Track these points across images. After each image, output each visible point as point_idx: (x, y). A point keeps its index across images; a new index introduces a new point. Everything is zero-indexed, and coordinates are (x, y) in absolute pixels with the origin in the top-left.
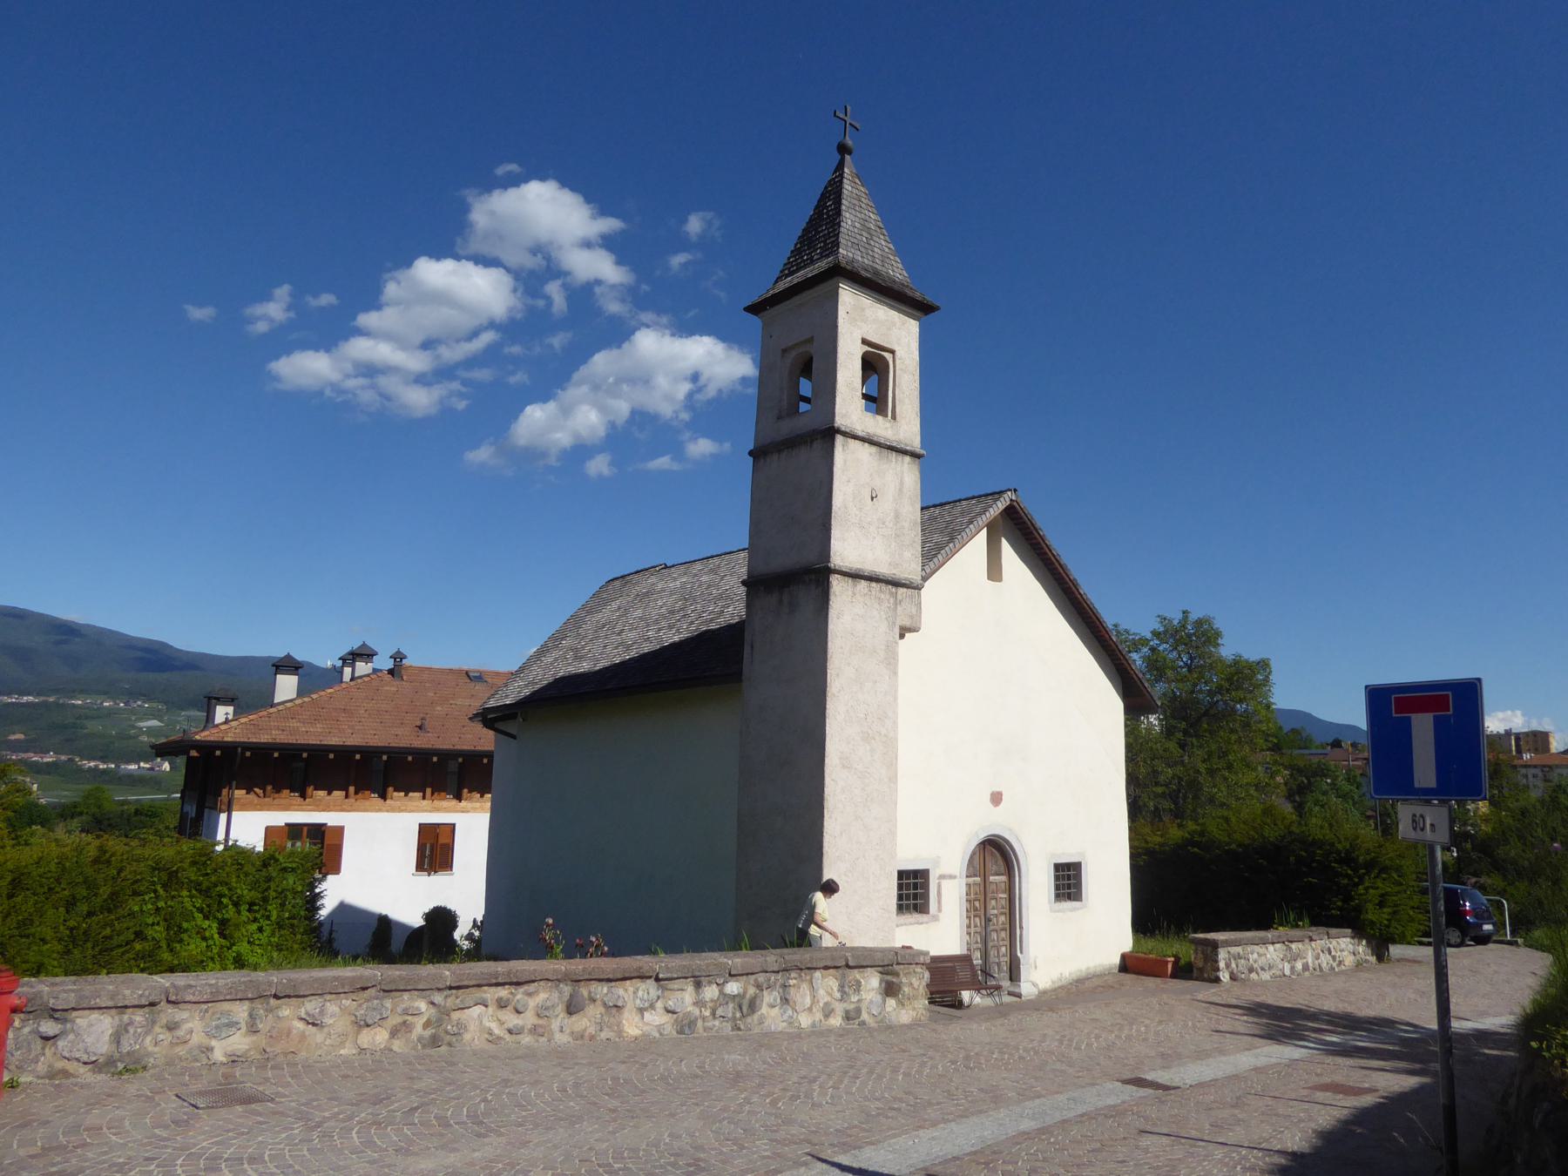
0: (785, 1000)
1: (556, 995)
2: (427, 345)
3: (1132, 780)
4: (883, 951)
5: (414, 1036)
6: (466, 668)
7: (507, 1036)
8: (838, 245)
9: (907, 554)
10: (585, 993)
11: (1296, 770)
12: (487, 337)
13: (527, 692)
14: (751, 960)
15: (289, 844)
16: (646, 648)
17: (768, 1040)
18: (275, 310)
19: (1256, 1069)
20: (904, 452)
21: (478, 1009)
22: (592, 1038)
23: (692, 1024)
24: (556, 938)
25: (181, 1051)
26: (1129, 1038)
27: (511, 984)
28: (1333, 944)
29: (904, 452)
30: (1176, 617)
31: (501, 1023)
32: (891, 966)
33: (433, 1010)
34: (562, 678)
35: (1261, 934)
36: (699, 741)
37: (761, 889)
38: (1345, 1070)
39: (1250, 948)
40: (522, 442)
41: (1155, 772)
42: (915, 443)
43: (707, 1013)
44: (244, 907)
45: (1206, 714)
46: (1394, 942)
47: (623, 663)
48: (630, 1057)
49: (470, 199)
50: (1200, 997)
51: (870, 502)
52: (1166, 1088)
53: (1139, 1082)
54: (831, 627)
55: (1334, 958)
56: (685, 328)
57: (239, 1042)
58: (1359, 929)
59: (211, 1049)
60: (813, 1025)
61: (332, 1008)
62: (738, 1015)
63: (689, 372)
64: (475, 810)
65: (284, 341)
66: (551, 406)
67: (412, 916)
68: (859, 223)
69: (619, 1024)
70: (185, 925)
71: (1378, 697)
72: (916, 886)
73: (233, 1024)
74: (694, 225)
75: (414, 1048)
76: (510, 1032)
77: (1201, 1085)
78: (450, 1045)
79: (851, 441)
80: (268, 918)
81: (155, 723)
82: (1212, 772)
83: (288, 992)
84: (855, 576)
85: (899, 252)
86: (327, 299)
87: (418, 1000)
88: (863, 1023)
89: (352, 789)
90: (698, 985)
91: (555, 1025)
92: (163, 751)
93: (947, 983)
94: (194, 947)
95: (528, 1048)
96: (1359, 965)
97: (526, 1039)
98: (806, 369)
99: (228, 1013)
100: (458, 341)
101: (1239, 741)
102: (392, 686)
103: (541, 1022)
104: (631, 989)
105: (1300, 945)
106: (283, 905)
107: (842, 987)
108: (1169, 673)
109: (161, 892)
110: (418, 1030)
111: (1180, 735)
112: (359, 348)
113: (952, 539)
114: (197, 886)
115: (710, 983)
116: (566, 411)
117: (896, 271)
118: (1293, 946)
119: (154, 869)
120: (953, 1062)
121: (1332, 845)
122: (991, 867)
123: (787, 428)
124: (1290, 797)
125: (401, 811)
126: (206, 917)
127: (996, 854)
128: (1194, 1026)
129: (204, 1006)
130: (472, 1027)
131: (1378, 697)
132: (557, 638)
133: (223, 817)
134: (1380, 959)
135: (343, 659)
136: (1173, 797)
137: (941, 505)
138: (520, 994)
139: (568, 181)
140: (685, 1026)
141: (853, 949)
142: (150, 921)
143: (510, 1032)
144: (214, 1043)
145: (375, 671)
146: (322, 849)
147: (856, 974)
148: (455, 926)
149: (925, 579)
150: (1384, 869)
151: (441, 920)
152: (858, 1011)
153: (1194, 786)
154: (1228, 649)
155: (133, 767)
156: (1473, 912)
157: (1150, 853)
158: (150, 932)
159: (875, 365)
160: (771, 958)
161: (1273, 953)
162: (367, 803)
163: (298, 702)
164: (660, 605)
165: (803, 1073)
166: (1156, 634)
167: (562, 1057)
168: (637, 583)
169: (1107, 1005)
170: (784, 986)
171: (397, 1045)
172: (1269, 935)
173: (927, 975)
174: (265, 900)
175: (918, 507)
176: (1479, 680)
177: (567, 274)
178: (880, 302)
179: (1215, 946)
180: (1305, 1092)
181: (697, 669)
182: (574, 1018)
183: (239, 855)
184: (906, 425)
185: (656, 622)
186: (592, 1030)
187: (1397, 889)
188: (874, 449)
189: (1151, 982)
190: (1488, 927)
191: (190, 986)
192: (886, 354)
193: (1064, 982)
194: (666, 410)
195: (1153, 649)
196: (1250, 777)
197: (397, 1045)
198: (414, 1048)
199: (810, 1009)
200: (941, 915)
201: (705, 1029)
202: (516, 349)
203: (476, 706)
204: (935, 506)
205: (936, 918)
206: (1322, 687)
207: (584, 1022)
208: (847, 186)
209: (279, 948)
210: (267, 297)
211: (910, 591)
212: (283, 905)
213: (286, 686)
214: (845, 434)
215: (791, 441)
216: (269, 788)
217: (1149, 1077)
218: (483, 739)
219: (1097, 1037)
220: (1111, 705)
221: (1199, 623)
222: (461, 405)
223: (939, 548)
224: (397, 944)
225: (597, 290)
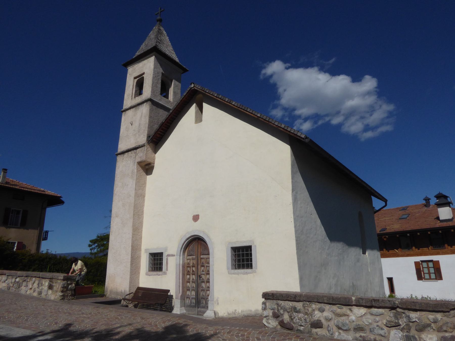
79: (127, 112)
127: (196, 245)
188: (134, 109)
193: (237, 315)
205: (165, 273)
214: (329, 80)
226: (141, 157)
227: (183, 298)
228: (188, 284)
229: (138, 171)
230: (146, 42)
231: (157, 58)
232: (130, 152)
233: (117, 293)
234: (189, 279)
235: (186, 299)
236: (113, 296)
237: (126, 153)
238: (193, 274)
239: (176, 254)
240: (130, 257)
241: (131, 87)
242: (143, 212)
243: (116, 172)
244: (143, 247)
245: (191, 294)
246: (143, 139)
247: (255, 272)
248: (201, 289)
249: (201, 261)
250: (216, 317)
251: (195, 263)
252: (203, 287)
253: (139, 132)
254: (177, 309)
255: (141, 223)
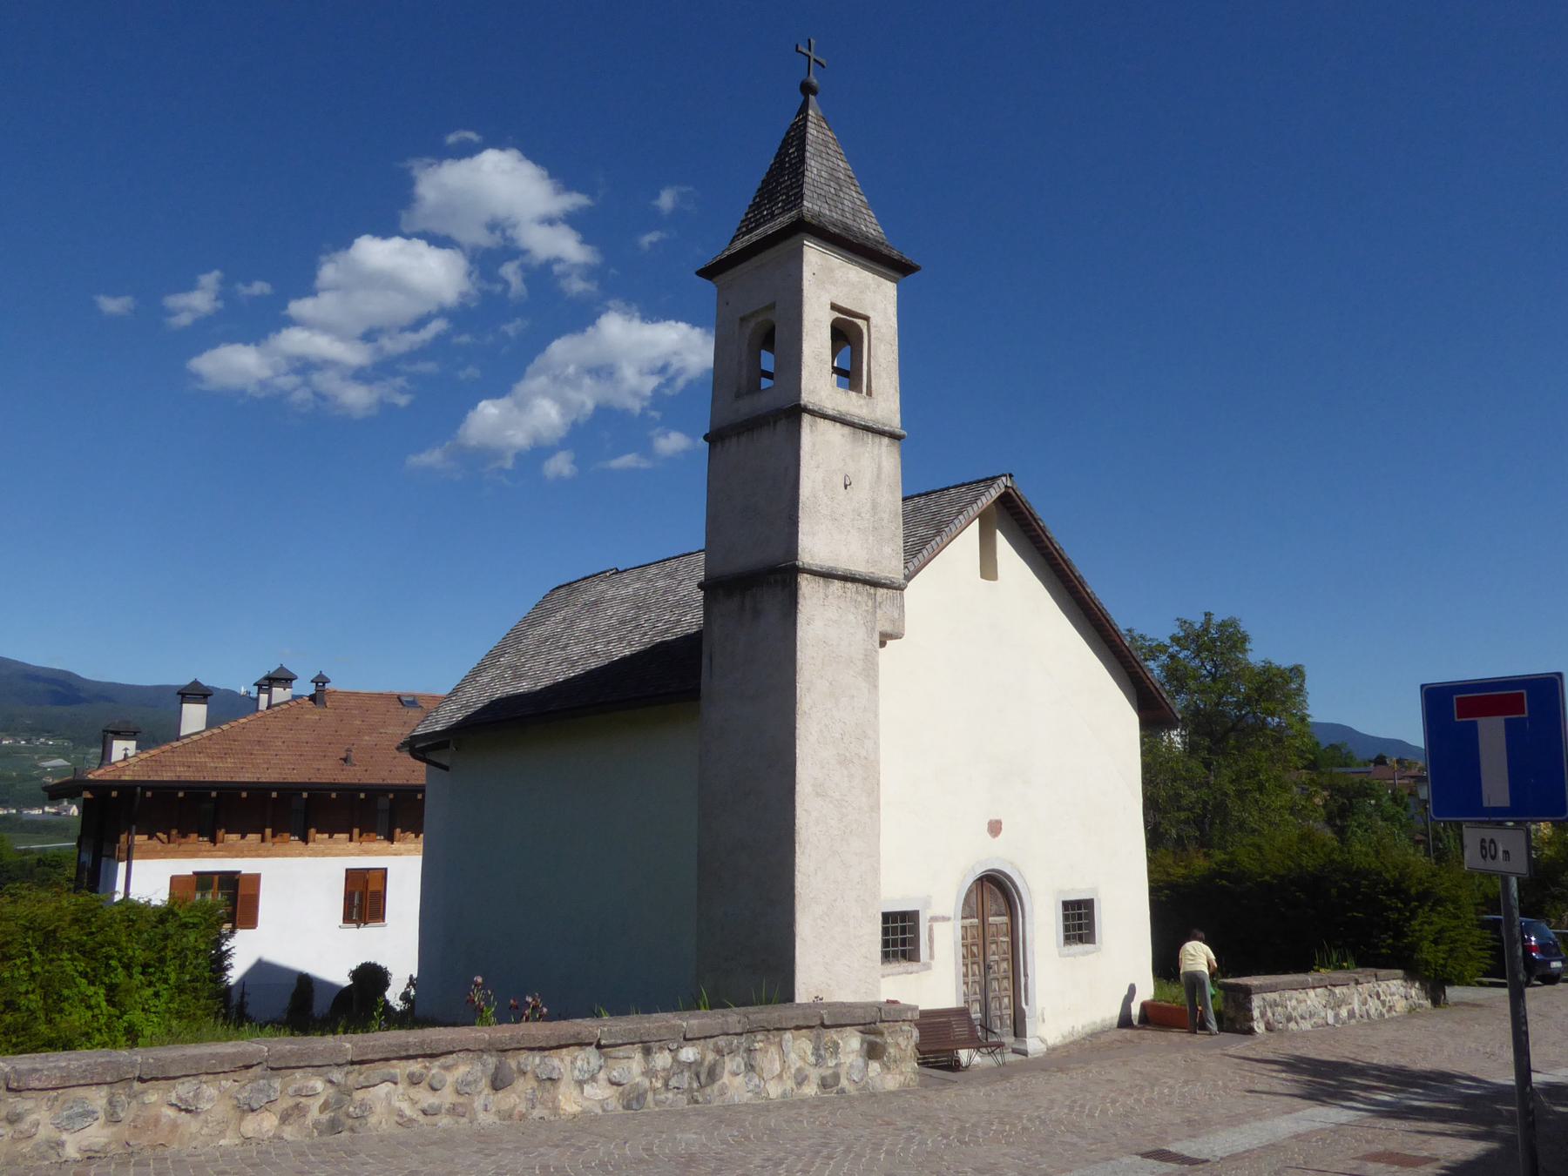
0: (750, 1067)
1: (479, 1067)
2: (369, 336)
3: (1151, 805)
4: (865, 1006)
5: (309, 1121)
6: (397, 691)
7: (421, 1118)
8: (801, 196)
9: (887, 550)
10: (513, 1065)
11: (1336, 790)
12: (437, 326)
13: (459, 716)
14: (706, 1021)
15: (198, 896)
16: (593, 664)
17: (730, 1114)
18: (200, 300)
19: (1297, 1136)
20: (882, 433)
21: (385, 1088)
22: (523, 1117)
23: (640, 1097)
24: (487, 999)
25: (25, 1147)
26: (1150, 1101)
27: (424, 1056)
28: (1382, 987)
29: (882, 433)
30: (1198, 621)
31: (414, 1102)
32: (873, 1024)
33: (331, 1090)
34: (500, 700)
35: (1301, 977)
36: (649, 772)
37: (721, 938)
38: (1399, 1135)
39: (1287, 994)
40: (473, 443)
41: (1178, 795)
42: (894, 421)
43: (659, 1084)
44: (137, 970)
45: (1233, 729)
46: (1451, 983)
47: (567, 681)
48: (566, 1139)
49: (415, 172)
50: (1231, 1051)
51: (844, 493)
52: (1192, 1161)
53: (1162, 1155)
54: (800, 633)
55: (1383, 1003)
56: (653, 313)
57: (97, 1134)
58: (1412, 971)
59: (61, 1144)
60: (784, 1095)
61: (209, 1090)
62: (695, 1085)
63: (660, 364)
64: (409, 852)
65: (208, 333)
66: (506, 402)
67: (339, 974)
68: (824, 164)
69: (555, 1099)
70: (66, 992)
71: (1437, 699)
72: (904, 930)
73: (89, 1114)
74: (666, 200)
75: (310, 1135)
76: (425, 1112)
77: (1234, 1157)
78: (352, 1130)
79: (820, 421)
80: (166, 981)
81: (60, 762)
82: (1241, 794)
83: (155, 1074)
84: (827, 575)
85: (873, 204)
86: (260, 288)
87: (316, 1077)
88: (843, 1091)
89: (268, 831)
90: (647, 1052)
91: (478, 1103)
92: (56, 794)
93: (940, 1042)
94: (77, 1017)
95: (445, 1130)
96: (1412, 1010)
97: (444, 1121)
98: (768, 339)
99: (83, 1100)
100: (403, 330)
101: (1271, 759)
102: (313, 714)
103: (461, 1100)
104: (568, 1059)
105: (1345, 989)
106: (182, 966)
107: (816, 1049)
108: (1191, 683)
109: (36, 955)
110: (314, 1114)
111: (1204, 754)
112: (295, 341)
113: (939, 532)
114: (80, 947)
115: (661, 1049)
116: (523, 405)
117: (870, 227)
118: (1337, 990)
119: (28, 929)
120: (945, 1136)
121: (1379, 874)
122: (991, 906)
123: (747, 407)
124: (1330, 821)
125: (324, 855)
126: (91, 983)
127: (995, 893)
128: (1225, 1087)
129: (54, 1093)
130: (379, 1108)
131: (1437, 699)
132: (494, 655)
133: (122, 866)
134: (1436, 1002)
135: (259, 685)
136: (1199, 822)
137: (927, 494)
138: (435, 1068)
139: (531, 153)
140: (633, 1099)
141: (830, 1005)
142: (22, 989)
143: (425, 1112)
144: (65, 1136)
145: (294, 698)
146: (236, 901)
147: (833, 1034)
148: (386, 985)
149: (908, 578)
150: (1439, 901)
151: (371, 978)
152: (836, 1077)
153: (1221, 809)
154: (1257, 655)
155: (37, 812)
156: (1542, 948)
157: (1172, 886)
158: (23, 1001)
159: (846, 334)
160: (733, 1017)
161: (1313, 999)
162: (286, 847)
163: (207, 734)
164: (612, 613)
165: (769, 1153)
166: (1175, 639)
167: (484, 1140)
168: (585, 591)
169: (1125, 1063)
170: (749, 1050)
171: (289, 1133)
172: (1309, 978)
173: (916, 1033)
174: (162, 960)
175: (900, 496)
176: (1560, 675)
177: (525, 252)
178: (851, 261)
179: (1247, 992)
180: (1354, 1164)
181: (652, 687)
182: (501, 1094)
183: (134, 912)
184: (884, 404)
185: (606, 634)
186: (522, 1108)
187: (1455, 923)
188: (847, 430)
189: (1175, 1036)
190: (1556, 965)
191: (35, 1070)
192: (859, 322)
193: (1076, 1037)
194: (636, 406)
195: (1172, 657)
196: (1283, 799)
197: (289, 1133)
198: (310, 1135)
199: (780, 1076)
201: (657, 1103)
202: (465, 339)
203: (404, 733)
204: (919, 495)
205: (928, 967)
206: (1369, 698)
207: (514, 1099)
208: (812, 131)
209: (179, 1015)
210: (190, 286)
211: (890, 592)
212: (182, 966)
213: (194, 717)
214: (813, 413)
215: (752, 422)
216: (174, 832)
217: (1174, 1148)
218: (413, 772)
219: (1114, 1102)
220: (1125, 721)
221: (1222, 626)
222: (403, 401)
223: (924, 542)
224: (321, 1006)
225: (557, 268)
232: (849, 585)
237: (837, 584)
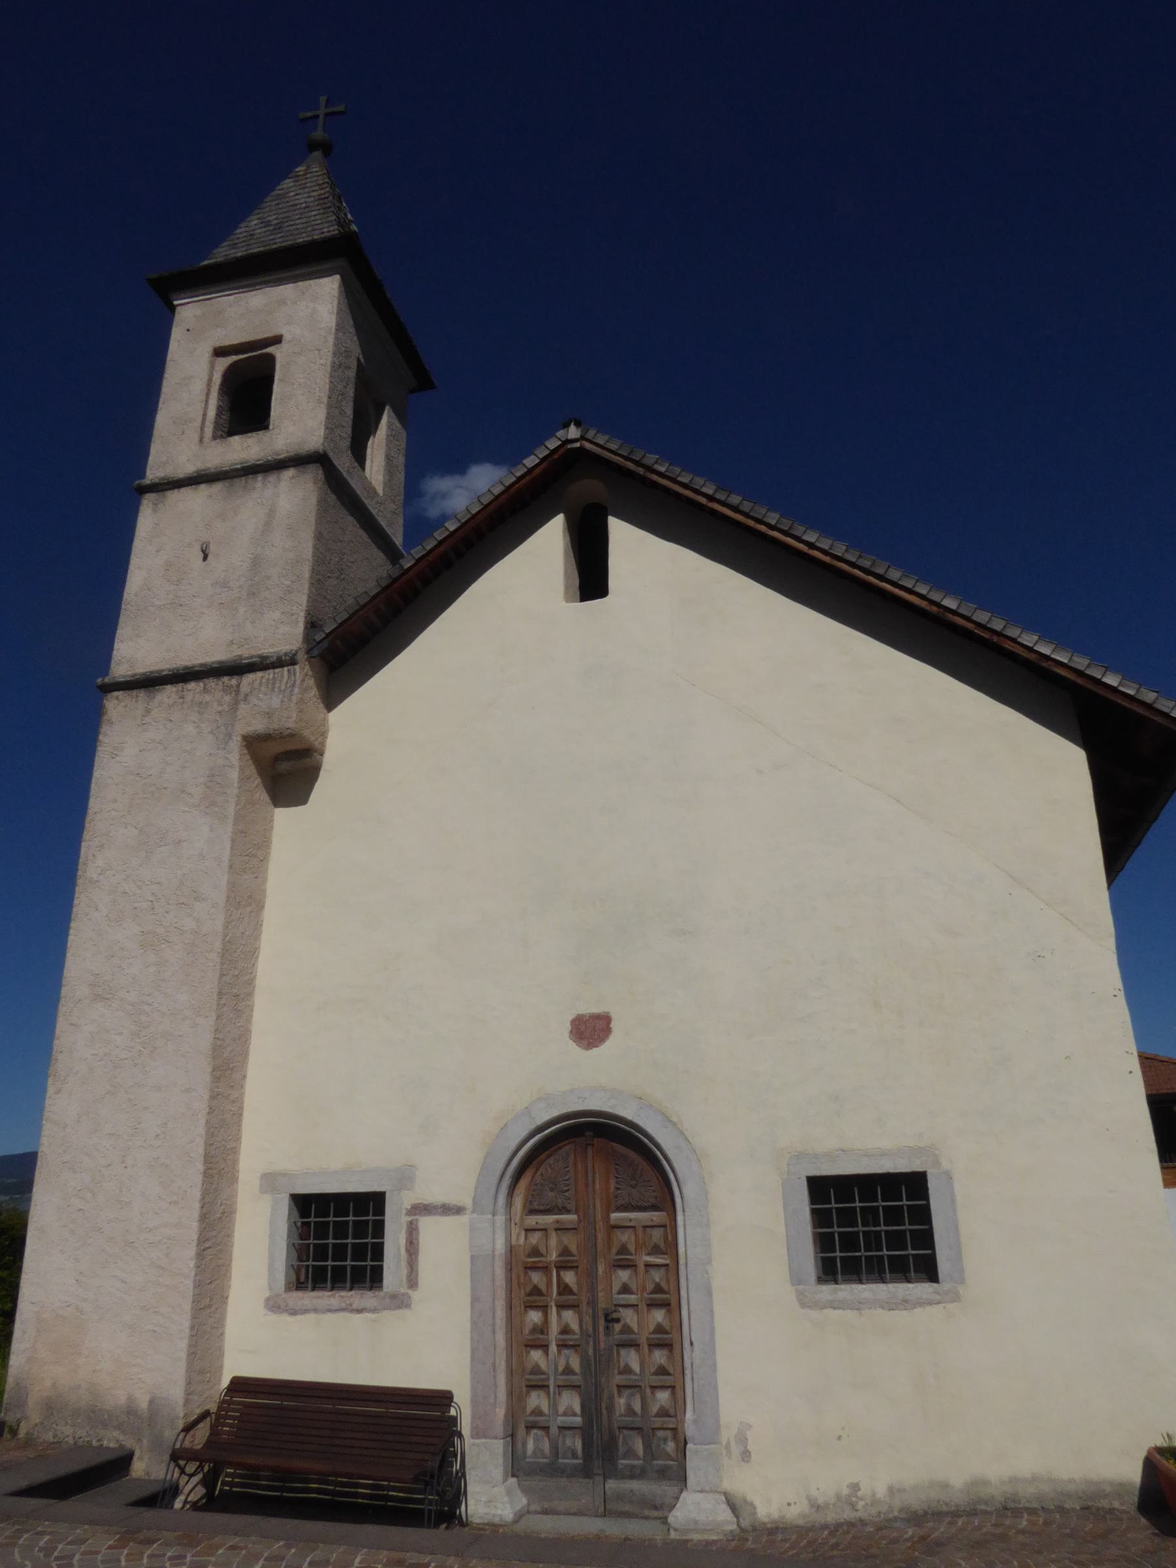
79: (173, 496)
127: (595, 1175)
188: (217, 487)
192: (269, 350)
200: (415, 1295)
205: (400, 1302)
226: (269, 715)
227: (519, 1424)
228: (536, 1355)
229: (243, 779)
230: (270, 211)
231: (347, 289)
232: (192, 685)
233: (96, 1416)
234: (542, 1329)
235: (521, 1431)
236: (68, 1430)
237: (170, 689)
238: (561, 1307)
239: (468, 1202)
240: (196, 1214)
241: (199, 386)
242: (251, 982)
243: (97, 773)
244: (252, 1162)
245: (554, 1406)
246: (281, 629)
247: (956, 1298)
248: (619, 1379)
249: (609, 1238)
250: (743, 1524)
251: (573, 1248)
252: (627, 1370)
253: (252, 594)
254: (490, 1494)
255: (243, 1038)
